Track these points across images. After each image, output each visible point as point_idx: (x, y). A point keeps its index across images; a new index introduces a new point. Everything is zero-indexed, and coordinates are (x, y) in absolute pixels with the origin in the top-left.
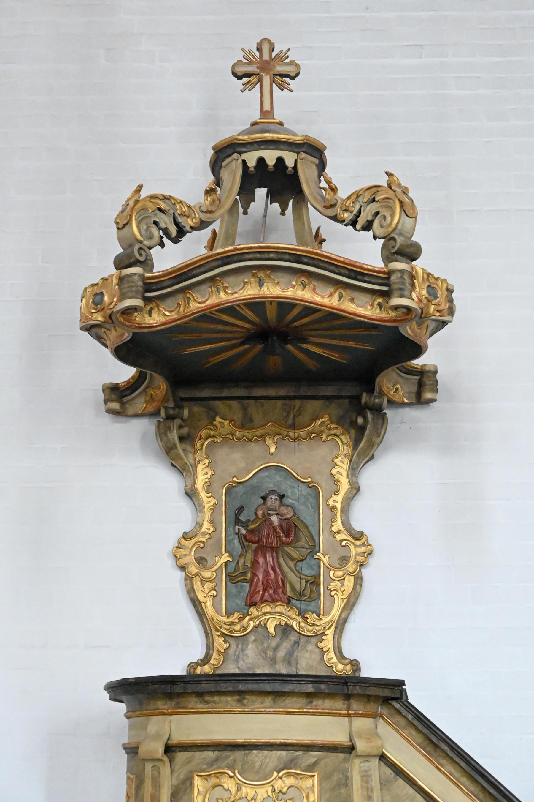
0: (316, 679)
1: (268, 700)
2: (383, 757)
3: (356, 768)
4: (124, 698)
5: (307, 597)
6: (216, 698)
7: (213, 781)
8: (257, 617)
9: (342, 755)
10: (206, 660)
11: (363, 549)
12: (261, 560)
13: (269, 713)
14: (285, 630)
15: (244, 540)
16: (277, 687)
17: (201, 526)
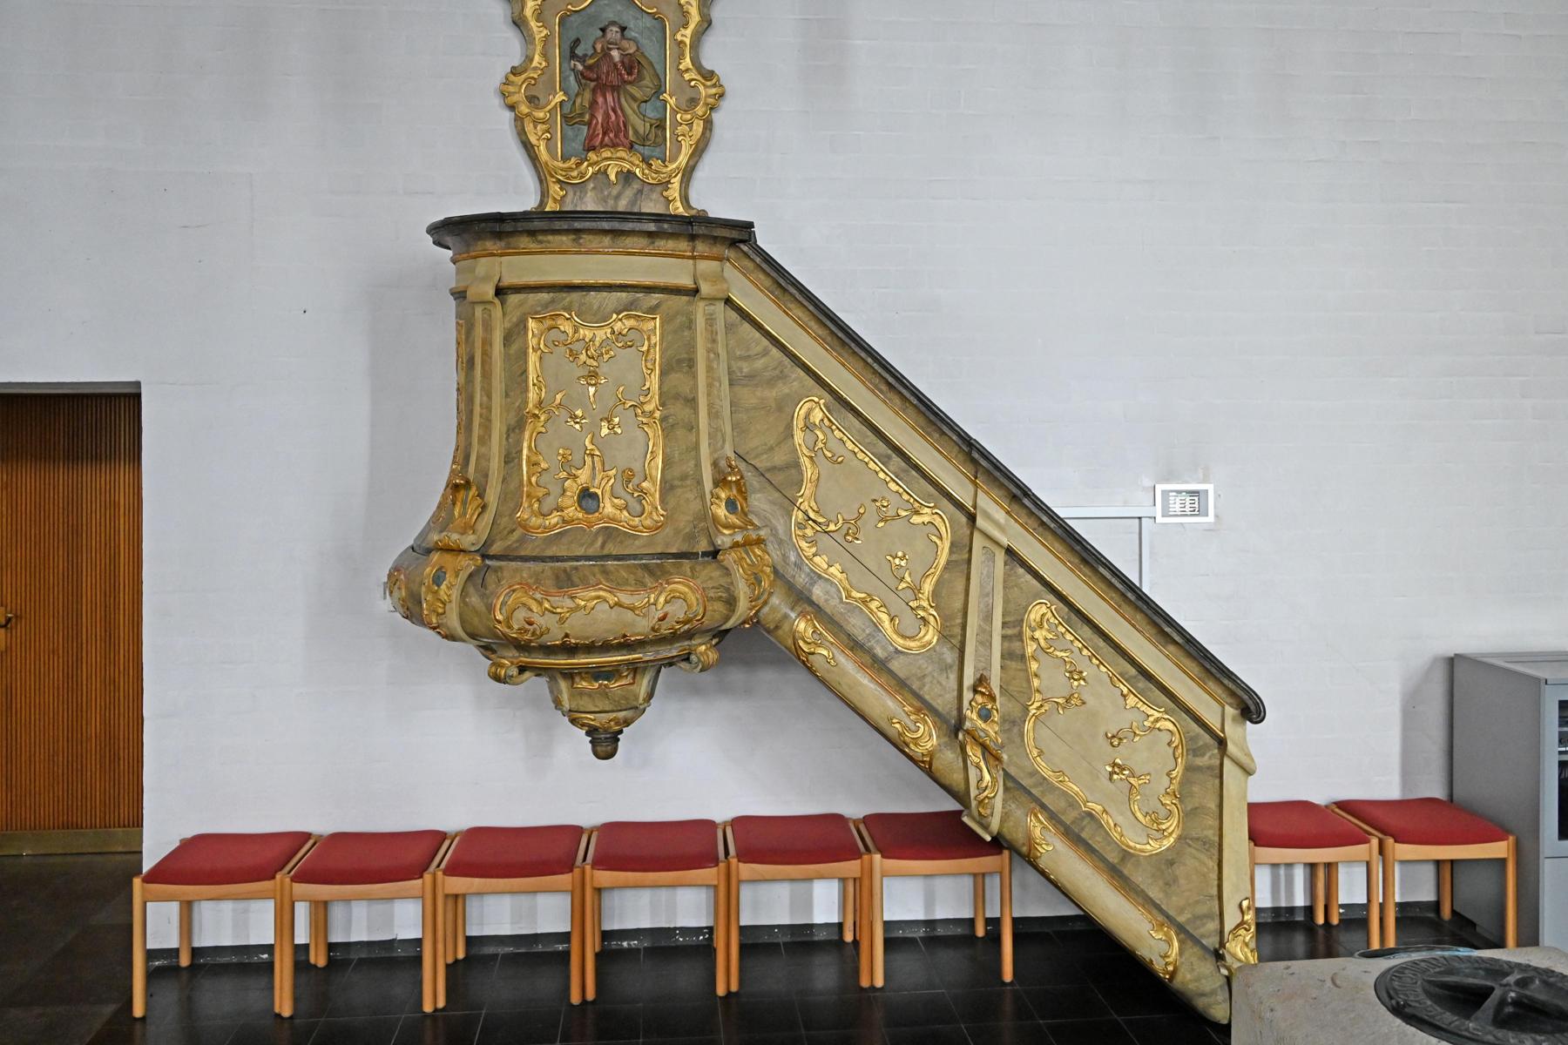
0: (658, 218)
1: (607, 240)
2: (728, 301)
3: (700, 310)
4: (449, 240)
5: (652, 142)
6: (550, 238)
7: (548, 323)
8: (596, 163)
9: (685, 298)
10: (542, 203)
11: (713, 91)
12: (600, 100)
13: (607, 253)
14: (627, 177)
15: (581, 77)
16: (616, 225)
17: (532, 60)
